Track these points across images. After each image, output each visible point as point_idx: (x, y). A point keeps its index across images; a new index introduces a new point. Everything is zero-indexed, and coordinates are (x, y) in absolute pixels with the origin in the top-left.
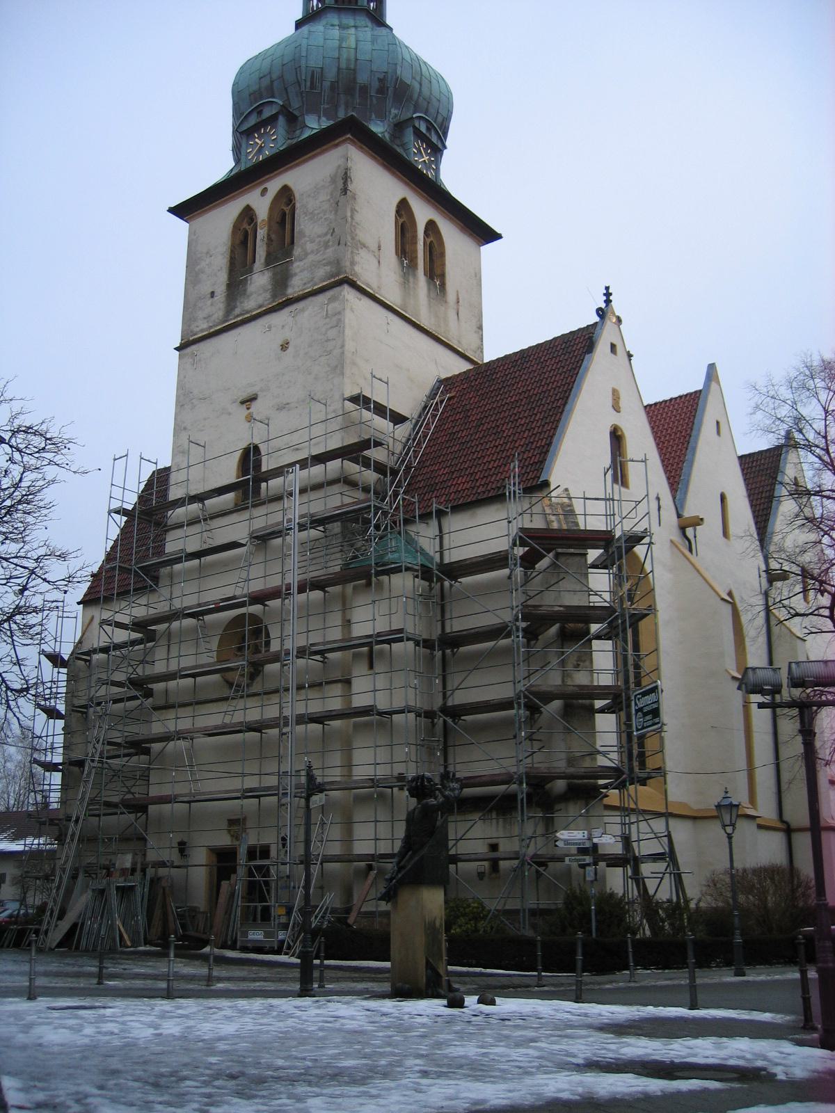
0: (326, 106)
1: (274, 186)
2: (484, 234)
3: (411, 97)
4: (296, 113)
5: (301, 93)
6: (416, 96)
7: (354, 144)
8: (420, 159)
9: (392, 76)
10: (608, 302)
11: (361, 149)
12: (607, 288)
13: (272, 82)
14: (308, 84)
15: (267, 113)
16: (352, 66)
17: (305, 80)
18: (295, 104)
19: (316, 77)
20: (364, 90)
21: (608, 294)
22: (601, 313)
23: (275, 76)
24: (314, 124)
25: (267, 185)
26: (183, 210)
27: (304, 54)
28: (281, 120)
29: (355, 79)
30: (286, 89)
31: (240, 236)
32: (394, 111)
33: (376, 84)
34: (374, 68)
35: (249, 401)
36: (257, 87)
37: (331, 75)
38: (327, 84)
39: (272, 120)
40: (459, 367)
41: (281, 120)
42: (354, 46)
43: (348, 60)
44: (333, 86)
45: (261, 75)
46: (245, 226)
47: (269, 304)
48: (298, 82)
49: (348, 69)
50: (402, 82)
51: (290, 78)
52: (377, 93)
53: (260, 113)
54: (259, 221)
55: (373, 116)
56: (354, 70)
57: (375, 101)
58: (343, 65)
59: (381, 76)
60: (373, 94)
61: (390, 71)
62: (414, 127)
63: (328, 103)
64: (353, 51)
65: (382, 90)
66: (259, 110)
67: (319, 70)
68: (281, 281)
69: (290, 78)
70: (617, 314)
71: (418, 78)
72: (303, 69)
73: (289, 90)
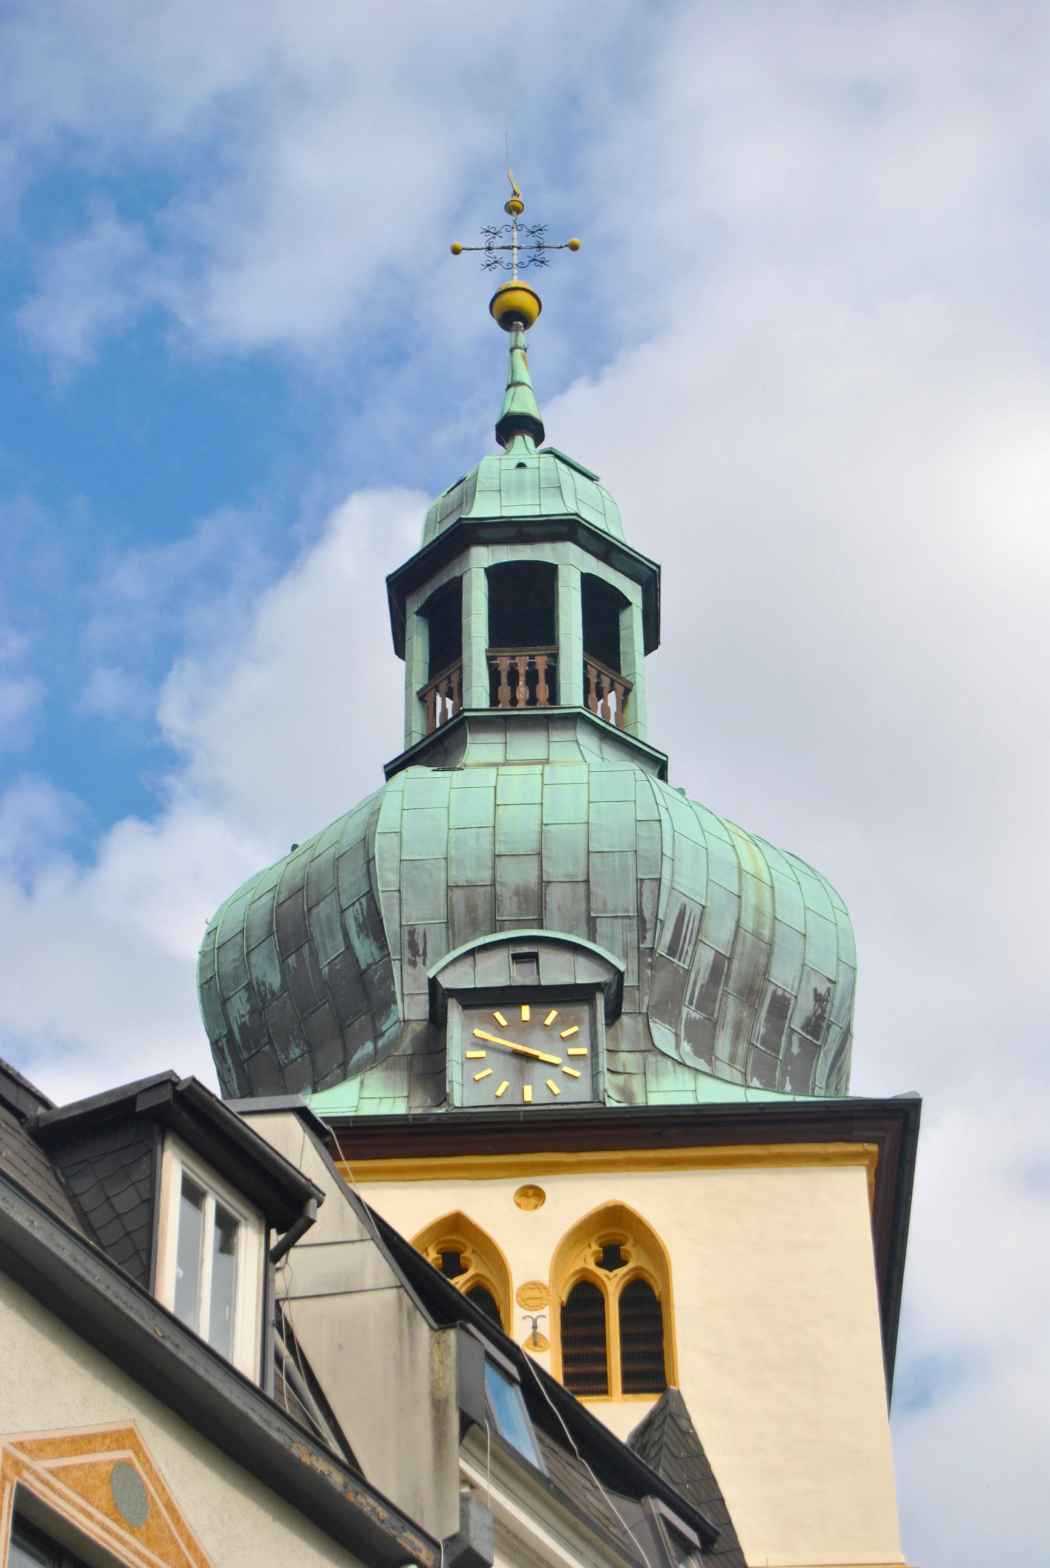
13: (543, 884)
14: (667, 936)
29: (766, 971)
54: (518, 1278)
67: (698, 910)
68: (361, 904)
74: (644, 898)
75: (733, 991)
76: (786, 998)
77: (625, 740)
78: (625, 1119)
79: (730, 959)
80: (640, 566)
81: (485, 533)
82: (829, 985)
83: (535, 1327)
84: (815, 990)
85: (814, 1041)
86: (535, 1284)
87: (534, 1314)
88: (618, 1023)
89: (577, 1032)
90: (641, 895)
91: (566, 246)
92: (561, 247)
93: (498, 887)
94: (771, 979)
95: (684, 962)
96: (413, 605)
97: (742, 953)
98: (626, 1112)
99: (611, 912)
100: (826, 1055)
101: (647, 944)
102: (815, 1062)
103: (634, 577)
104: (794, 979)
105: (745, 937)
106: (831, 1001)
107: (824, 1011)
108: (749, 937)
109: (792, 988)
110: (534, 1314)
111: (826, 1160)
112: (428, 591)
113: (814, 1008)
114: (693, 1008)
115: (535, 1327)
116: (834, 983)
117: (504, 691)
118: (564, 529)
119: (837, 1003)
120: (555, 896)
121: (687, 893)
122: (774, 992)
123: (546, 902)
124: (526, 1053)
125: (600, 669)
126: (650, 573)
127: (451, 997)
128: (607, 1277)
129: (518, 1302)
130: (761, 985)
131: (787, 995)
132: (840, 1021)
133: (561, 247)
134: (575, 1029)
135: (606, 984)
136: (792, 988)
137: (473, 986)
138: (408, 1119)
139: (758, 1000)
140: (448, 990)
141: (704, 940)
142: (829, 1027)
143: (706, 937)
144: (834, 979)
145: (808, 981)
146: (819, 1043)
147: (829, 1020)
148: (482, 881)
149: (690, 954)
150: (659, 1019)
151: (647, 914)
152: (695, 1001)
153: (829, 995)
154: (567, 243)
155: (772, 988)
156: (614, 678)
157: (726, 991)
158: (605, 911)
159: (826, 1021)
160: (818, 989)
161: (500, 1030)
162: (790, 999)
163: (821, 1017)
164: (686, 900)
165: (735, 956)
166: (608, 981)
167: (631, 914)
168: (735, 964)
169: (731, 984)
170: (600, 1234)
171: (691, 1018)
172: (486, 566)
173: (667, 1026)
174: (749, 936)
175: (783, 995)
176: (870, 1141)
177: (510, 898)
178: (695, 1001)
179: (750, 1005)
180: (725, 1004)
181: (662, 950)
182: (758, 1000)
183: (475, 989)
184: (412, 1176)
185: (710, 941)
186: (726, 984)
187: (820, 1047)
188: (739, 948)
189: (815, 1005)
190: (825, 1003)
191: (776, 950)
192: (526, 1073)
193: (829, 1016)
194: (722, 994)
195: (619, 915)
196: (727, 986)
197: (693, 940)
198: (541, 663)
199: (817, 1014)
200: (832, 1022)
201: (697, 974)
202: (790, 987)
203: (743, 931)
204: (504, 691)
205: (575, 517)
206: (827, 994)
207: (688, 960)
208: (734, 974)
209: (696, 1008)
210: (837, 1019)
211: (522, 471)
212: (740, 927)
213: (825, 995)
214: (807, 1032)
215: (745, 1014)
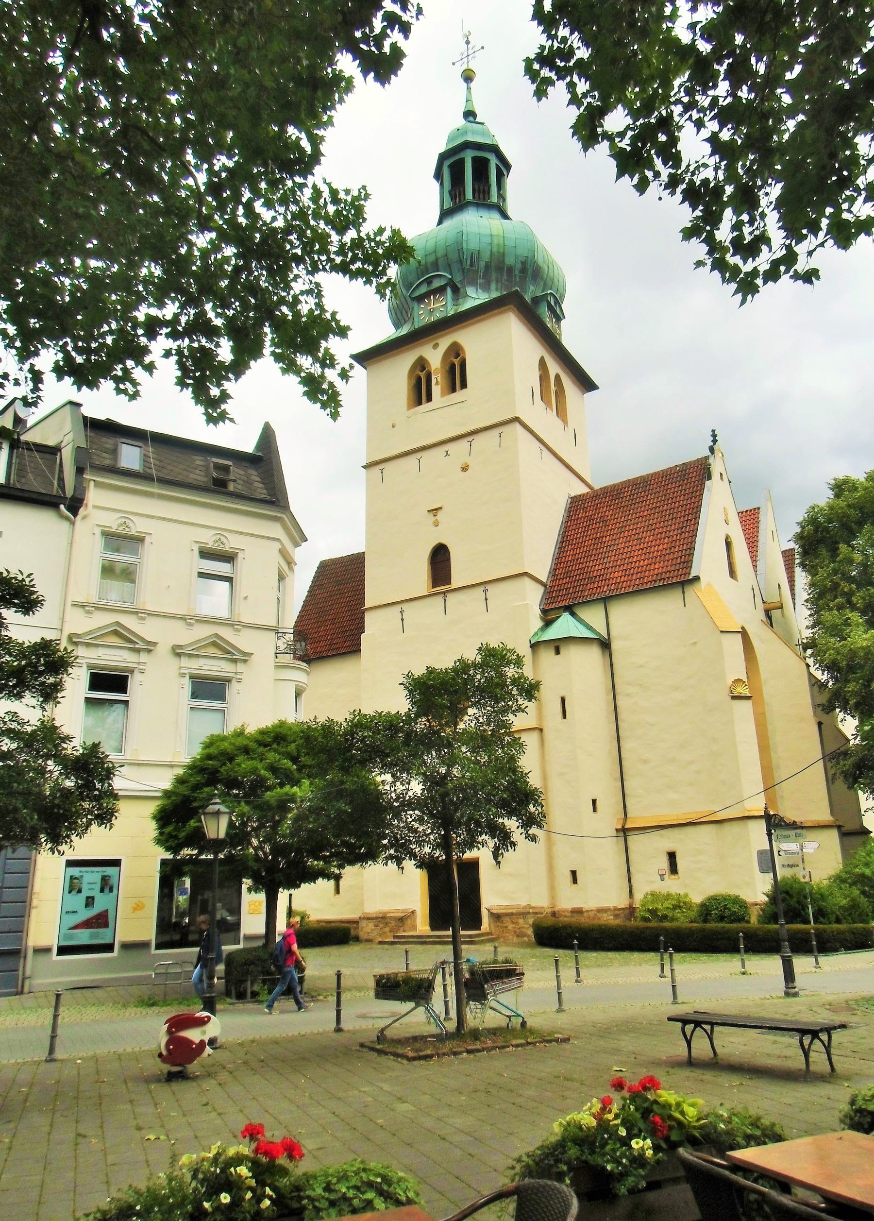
1: (445, 342)
2: (587, 384)
3: (542, 279)
4: (459, 286)
5: (463, 269)
6: (545, 276)
7: (514, 312)
8: (550, 323)
10: (715, 441)
11: (518, 316)
12: (713, 431)
13: (437, 259)
14: (469, 263)
15: (437, 284)
16: (501, 251)
18: (458, 279)
19: (475, 257)
20: (510, 270)
21: (714, 436)
22: (712, 450)
23: (439, 254)
24: (475, 297)
25: (439, 341)
28: (449, 291)
29: (504, 260)
30: (449, 265)
31: (414, 381)
32: (532, 288)
35: (435, 511)
37: (486, 256)
38: (482, 264)
39: (441, 290)
41: (449, 291)
44: (487, 266)
49: (498, 252)
50: (538, 265)
51: (454, 257)
55: (223, 245)
57: (518, 280)
58: (495, 250)
59: (523, 260)
60: (517, 273)
65: (524, 270)
69: (454, 257)
70: (293, 380)
72: (465, 251)
96: (447, 163)
112: (452, 160)
117: (476, 195)
181: (468, 267)
204: (476, 195)
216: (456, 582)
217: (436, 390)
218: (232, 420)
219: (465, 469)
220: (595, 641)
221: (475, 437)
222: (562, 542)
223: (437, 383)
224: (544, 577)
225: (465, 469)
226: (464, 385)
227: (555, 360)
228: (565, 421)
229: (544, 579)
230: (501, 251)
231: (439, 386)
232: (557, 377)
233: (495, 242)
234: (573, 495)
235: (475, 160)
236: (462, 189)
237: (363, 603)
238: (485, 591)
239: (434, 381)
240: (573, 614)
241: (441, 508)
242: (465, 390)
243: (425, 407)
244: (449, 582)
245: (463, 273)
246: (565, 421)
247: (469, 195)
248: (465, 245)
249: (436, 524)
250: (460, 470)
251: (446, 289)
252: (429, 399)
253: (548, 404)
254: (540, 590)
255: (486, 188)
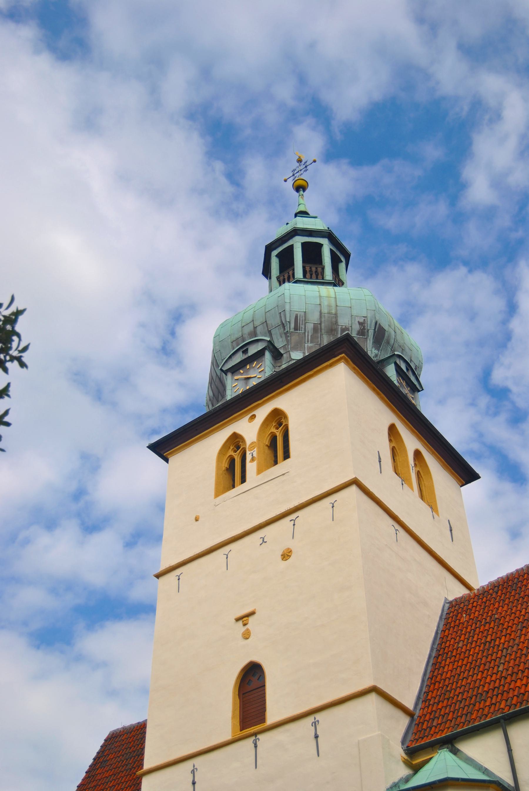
0: (310, 345)
3: (388, 342)
4: (282, 351)
5: (286, 334)
6: (392, 341)
7: (347, 363)
9: (371, 321)
13: (255, 328)
14: (293, 325)
15: (253, 350)
16: (333, 311)
17: (289, 322)
18: (279, 343)
26: (167, 460)
27: (287, 301)
28: (268, 355)
29: (336, 322)
31: (225, 464)
33: (356, 327)
34: (354, 313)
35: (243, 619)
36: (240, 334)
37: (314, 318)
39: (260, 355)
40: (460, 592)
41: (268, 355)
42: (333, 296)
43: (329, 306)
45: (243, 324)
46: (231, 453)
47: (394, 347)
48: (283, 324)
49: (329, 313)
52: (357, 335)
53: (245, 352)
54: (248, 442)
56: (336, 314)
58: (325, 310)
59: (361, 320)
61: (369, 315)
62: (396, 364)
63: (311, 342)
64: (333, 300)
66: (244, 349)
67: (303, 314)
69: (274, 321)
71: (393, 327)
73: (273, 332)
74: (282, 318)
75: (325, 333)
76: (347, 328)
77: (317, 281)
78: (269, 382)
79: (320, 324)
80: (323, 233)
81: (274, 246)
82: (364, 318)
83: (252, 455)
84: (359, 322)
85: (363, 337)
86: (252, 443)
87: (252, 452)
88: (282, 358)
89: (261, 364)
90: (281, 317)
91: (313, 162)
92: (311, 164)
93: (244, 335)
94: (339, 324)
95: (302, 331)
96: (275, 253)
97: (324, 321)
98: (268, 379)
99: (274, 326)
100: (370, 340)
101: (286, 330)
102: (366, 344)
103: (323, 237)
104: (349, 321)
105: (324, 315)
106: (366, 322)
107: (364, 327)
108: (326, 315)
109: (349, 324)
110: (252, 452)
111: (331, 366)
113: (360, 327)
114: (309, 343)
115: (252, 455)
116: (366, 317)
118: (293, 233)
119: (369, 323)
120: (259, 330)
121: (297, 310)
122: (341, 328)
123: (257, 333)
124: (248, 377)
125: (310, 266)
126: (328, 233)
127: (228, 372)
128: (277, 431)
129: (248, 450)
130: (336, 327)
131: (347, 327)
132: (372, 328)
133: (311, 164)
134: (261, 364)
135: (266, 347)
136: (349, 324)
137: (232, 366)
138: (211, 412)
139: (336, 332)
140: (226, 370)
141: (308, 322)
142: (368, 331)
143: (308, 321)
144: (366, 316)
145: (355, 320)
146: (366, 337)
147: (367, 329)
148: (240, 336)
149: (303, 327)
150: (295, 350)
151: (284, 322)
152: (309, 341)
153: (365, 321)
154: (312, 161)
155: (340, 327)
156: (316, 267)
157: (322, 334)
158: (272, 327)
159: (366, 329)
160: (359, 321)
161: (242, 374)
162: (349, 328)
163: (364, 329)
164: (297, 312)
165: (322, 322)
166: (266, 345)
167: (279, 324)
168: (323, 325)
169: (323, 331)
170: (275, 420)
171: (309, 346)
172: (275, 255)
173: (299, 352)
174: (326, 315)
175: (345, 327)
176: (341, 354)
177: (247, 337)
178: (309, 341)
179: (332, 335)
180: (322, 338)
181: (292, 330)
182: (336, 332)
183: (233, 366)
184: (428, 450)
185: (310, 321)
186: (321, 331)
187: (367, 338)
188: (323, 320)
189: (360, 326)
190: (364, 324)
191: (339, 315)
192: (248, 383)
193: (367, 327)
194: (320, 335)
195: (276, 326)
196: (322, 332)
197: (303, 323)
198: (291, 273)
199: (361, 328)
200: (369, 329)
201: (308, 332)
202: (348, 324)
203: (323, 314)
204: (308, 275)
205: (294, 228)
206: (364, 321)
207: (303, 329)
208: (323, 327)
209: (310, 343)
210: (371, 328)
211: (288, 225)
212: (321, 313)
213: (363, 322)
214: (360, 336)
215: (332, 338)
216: (271, 718)
217: (251, 467)
218: (194, 766)
219: (286, 555)
220: (493, 785)
221: (299, 513)
222: (437, 657)
223: (253, 459)
224: (409, 703)
225: (286, 555)
226: (287, 455)
227: (413, 432)
228: (433, 507)
229: (409, 703)
230: (333, 311)
231: (255, 463)
232: (417, 454)
233: (325, 303)
234: (451, 598)
235: (304, 245)
236: (291, 273)
237: (141, 766)
238: (315, 724)
239: (249, 457)
240: (455, 752)
241: (253, 613)
242: (288, 460)
243: (240, 488)
244: (262, 719)
245: (287, 337)
246: (433, 507)
247: (299, 273)
248: (287, 308)
249: (246, 636)
250: (280, 558)
251: (263, 354)
252: (243, 480)
253: (405, 480)
254: (404, 721)
255: (319, 270)
